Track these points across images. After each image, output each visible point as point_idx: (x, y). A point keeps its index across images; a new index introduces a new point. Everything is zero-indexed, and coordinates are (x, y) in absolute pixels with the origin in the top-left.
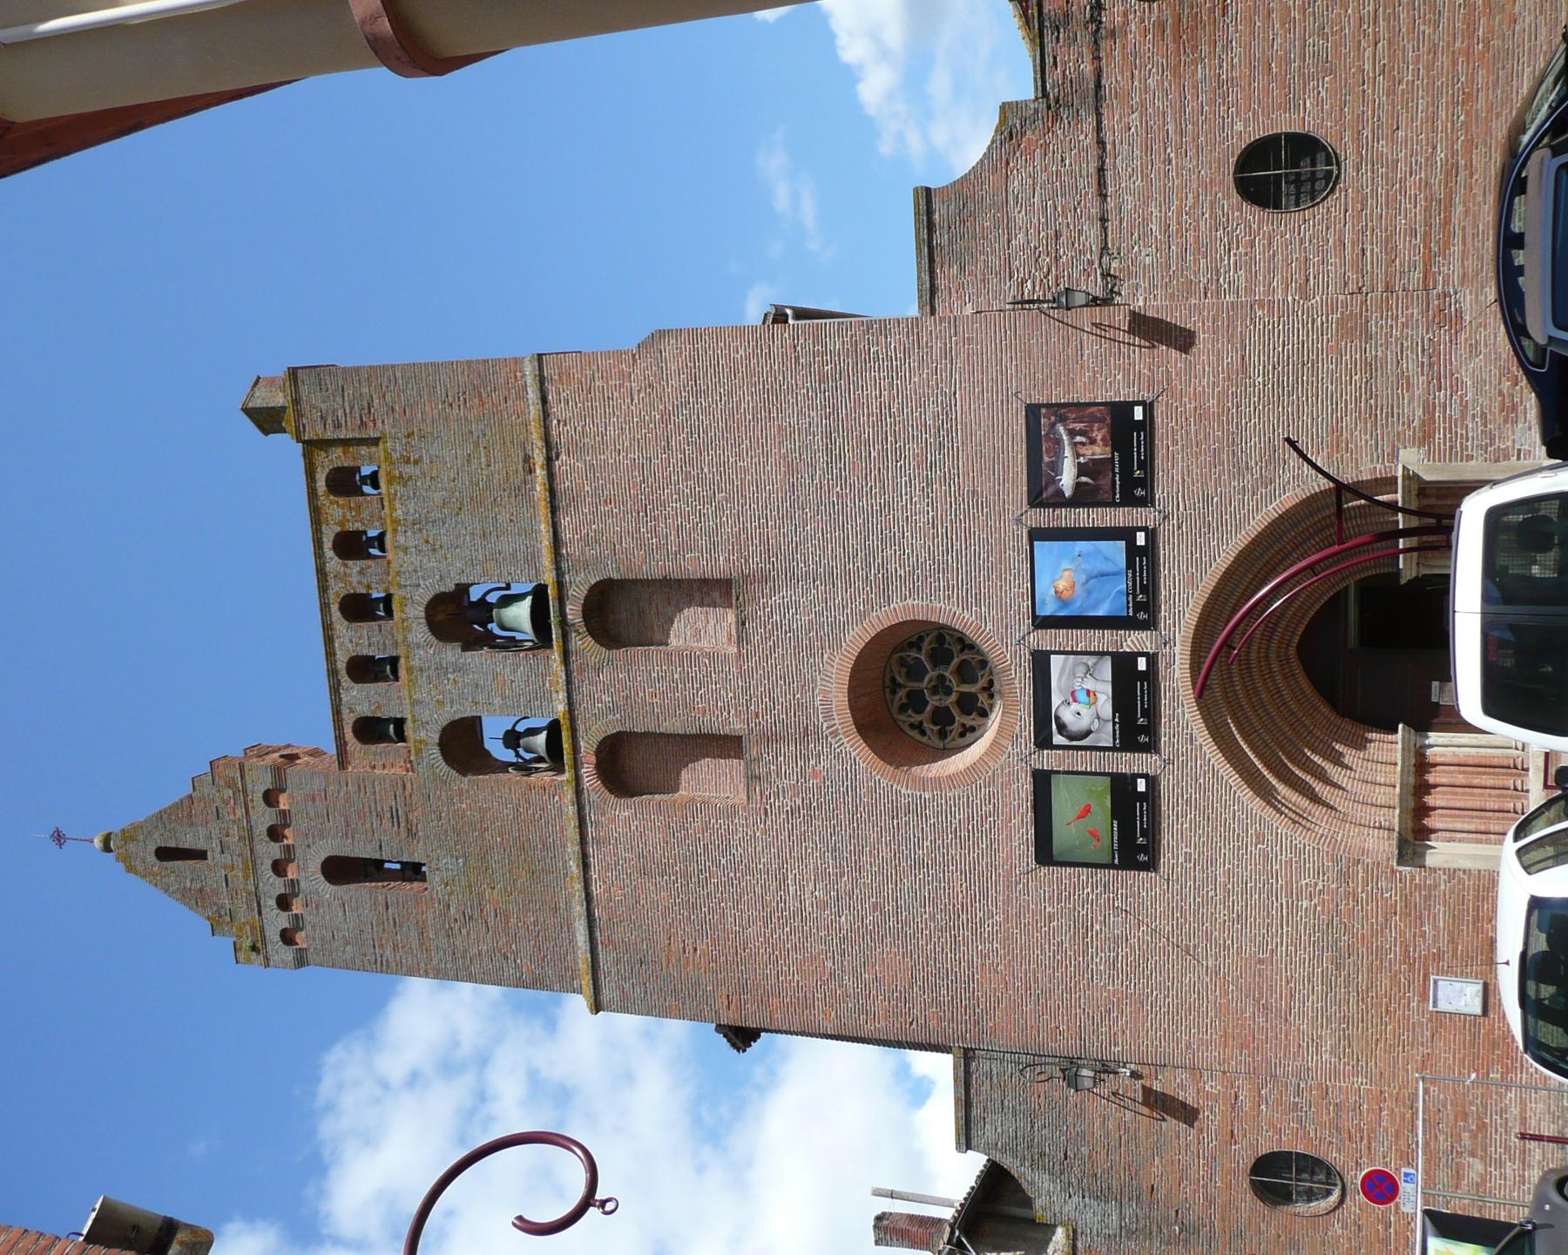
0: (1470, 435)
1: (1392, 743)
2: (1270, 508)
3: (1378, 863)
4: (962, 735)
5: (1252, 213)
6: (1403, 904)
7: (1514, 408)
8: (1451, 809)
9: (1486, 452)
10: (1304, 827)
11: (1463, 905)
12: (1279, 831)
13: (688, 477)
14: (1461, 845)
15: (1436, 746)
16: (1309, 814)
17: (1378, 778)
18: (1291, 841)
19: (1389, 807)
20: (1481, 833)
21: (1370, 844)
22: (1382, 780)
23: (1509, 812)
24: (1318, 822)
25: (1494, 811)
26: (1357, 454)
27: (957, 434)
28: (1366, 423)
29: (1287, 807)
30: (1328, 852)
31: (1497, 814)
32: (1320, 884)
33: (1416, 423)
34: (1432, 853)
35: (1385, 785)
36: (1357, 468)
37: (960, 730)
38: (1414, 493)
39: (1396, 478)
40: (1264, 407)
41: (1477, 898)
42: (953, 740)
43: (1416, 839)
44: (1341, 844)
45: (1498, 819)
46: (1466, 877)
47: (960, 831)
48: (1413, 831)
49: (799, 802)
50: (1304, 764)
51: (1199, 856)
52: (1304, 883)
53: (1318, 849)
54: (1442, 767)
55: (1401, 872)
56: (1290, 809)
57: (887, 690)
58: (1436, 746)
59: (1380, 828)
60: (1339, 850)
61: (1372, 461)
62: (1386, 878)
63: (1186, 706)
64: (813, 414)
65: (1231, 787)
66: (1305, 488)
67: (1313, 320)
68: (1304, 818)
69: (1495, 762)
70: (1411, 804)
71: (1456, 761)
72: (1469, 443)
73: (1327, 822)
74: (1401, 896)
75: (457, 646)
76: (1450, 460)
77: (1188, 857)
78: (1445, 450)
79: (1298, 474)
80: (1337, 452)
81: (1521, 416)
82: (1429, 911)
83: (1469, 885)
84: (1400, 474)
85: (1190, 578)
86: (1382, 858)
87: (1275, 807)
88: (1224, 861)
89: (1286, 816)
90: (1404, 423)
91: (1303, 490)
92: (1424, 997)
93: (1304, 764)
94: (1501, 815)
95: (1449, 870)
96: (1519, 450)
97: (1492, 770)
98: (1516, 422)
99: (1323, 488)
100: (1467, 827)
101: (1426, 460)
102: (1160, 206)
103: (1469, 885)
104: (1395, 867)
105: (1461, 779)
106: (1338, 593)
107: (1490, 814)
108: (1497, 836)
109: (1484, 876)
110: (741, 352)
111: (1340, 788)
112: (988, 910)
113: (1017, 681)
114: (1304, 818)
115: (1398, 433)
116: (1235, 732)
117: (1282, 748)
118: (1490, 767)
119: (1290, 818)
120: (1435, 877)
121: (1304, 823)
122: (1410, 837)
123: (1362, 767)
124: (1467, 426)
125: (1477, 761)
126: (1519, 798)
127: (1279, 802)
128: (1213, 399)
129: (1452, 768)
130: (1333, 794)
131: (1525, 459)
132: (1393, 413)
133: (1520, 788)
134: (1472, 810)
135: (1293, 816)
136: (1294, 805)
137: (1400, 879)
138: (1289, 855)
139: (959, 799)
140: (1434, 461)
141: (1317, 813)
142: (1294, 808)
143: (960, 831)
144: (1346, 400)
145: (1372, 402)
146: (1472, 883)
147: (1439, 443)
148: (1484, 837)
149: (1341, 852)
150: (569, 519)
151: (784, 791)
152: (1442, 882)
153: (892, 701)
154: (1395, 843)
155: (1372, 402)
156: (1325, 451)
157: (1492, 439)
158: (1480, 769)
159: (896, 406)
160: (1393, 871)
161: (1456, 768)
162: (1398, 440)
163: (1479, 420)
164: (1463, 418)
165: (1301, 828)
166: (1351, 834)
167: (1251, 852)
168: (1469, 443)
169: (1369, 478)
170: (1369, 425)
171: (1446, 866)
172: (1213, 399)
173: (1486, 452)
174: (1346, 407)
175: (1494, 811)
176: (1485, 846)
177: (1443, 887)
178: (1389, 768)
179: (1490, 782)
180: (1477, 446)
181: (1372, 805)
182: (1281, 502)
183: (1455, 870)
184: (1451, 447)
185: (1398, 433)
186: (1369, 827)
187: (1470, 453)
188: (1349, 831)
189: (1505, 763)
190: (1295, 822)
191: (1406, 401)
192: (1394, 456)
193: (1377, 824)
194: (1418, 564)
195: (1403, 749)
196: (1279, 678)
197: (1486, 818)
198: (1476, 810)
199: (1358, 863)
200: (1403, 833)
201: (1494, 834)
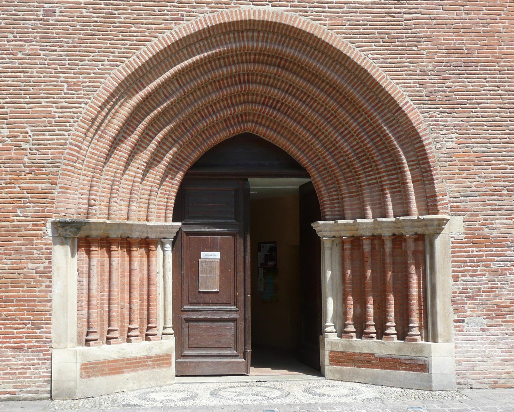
0: (476, 278)
1: (166, 217)
2: (408, 99)
3: (52, 203)
6: (10, 228)
7: (500, 316)
8: (110, 272)
9: (461, 292)
10: (88, 130)
11: (12, 287)
12: (83, 105)
14: (76, 283)
15: (130, 261)
16: (101, 136)
17: (135, 204)
19: (109, 214)
20: (89, 301)
21: (73, 195)
22: (134, 208)
23: (109, 325)
24: (92, 145)
25: (109, 311)
26: (458, 178)
28: (486, 186)
29: (107, 114)
30: (62, 153)
31: (106, 314)
32: (27, 146)
33: (486, 231)
34: (67, 252)
35: (129, 210)
36: (446, 178)
38: (420, 231)
39: (436, 213)
40: (500, 95)
41: (21, 299)
43: (80, 239)
44: (73, 166)
45: (102, 316)
46: (43, 288)
48: (88, 236)
50: (147, 134)
51: (52, 25)
52: (28, 129)
54: (146, 263)
55: (45, 225)
56: (105, 117)
58: (130, 261)
59: (89, 205)
60: (65, 164)
61: (452, 192)
62: (38, 211)
63: (211, 15)
65: (127, 58)
66: (427, 131)
68: (97, 130)
69: (153, 310)
70: (113, 235)
71: (153, 275)
72: (468, 278)
73: (93, 153)
74: (18, 226)
76: (453, 262)
78: (463, 257)
79: (440, 125)
80: (460, 161)
81: (493, 322)
82: (5, 254)
83: (35, 292)
84: (439, 216)
85: (340, 23)
86: (60, 207)
87: (107, 101)
88: (47, 50)
89: (99, 112)
90: (486, 220)
91: (425, 129)
93: (147, 134)
94: (106, 318)
95: (50, 272)
96: (463, 321)
97: (145, 307)
98: (487, 318)
99: (426, 147)
100: (94, 288)
101: (453, 240)
103: (35, 292)
104: (50, 220)
105: (136, 280)
106: (304, 170)
107: (106, 307)
108: (86, 315)
109: (45, 306)
111: (126, 168)
114: (97, 130)
115: (477, 215)
116: (194, 59)
117: (180, 100)
118: (149, 305)
119: (97, 116)
120: (40, 258)
121: (92, 130)
122: (82, 233)
123: (144, 189)
124: (483, 275)
125: (153, 293)
126: (122, 334)
127: (113, 107)
128: (508, 49)
129: (145, 272)
130: (119, 160)
131: (455, 327)
132: (495, 210)
133: (131, 334)
134: (110, 292)
135: (99, 120)
136: (110, 121)
137: (36, 225)
138: (57, 115)
140: (453, 247)
141: (101, 144)
142: (106, 121)
144: (506, 169)
145: (505, 192)
146: (37, 294)
147: (469, 251)
148: (85, 303)
149: (63, 166)
152: (35, 266)
154: (75, 218)
155: (505, 192)
156: (461, 150)
157: (473, 298)
158: (145, 297)
160: (44, 218)
161: (146, 276)
162: (472, 215)
163: (490, 285)
164: (491, 272)
165: (248, 27)
166: (82, 177)
167: (60, 77)
168: (468, 278)
169: (436, 190)
170: (484, 189)
171: (54, 269)
172: (508, 49)
173: (461, 292)
174: (500, 169)
175: (109, 311)
176: (76, 304)
177: (30, 266)
178: (143, 215)
179: (136, 307)
180: (466, 285)
181: (110, 198)
182: (414, 109)
183: (50, 277)
184: (465, 262)
185: (477, 215)
186: (90, 195)
187: (460, 278)
188: (85, 175)
189: (152, 319)
190: (93, 120)
191: (505, 221)
192: (457, 212)
193: (93, 202)
194: (334, 237)
195: (163, 227)
196: (228, 112)
197: (103, 304)
198: (110, 295)
199: (52, 184)
200: (87, 226)
201: (89, 314)
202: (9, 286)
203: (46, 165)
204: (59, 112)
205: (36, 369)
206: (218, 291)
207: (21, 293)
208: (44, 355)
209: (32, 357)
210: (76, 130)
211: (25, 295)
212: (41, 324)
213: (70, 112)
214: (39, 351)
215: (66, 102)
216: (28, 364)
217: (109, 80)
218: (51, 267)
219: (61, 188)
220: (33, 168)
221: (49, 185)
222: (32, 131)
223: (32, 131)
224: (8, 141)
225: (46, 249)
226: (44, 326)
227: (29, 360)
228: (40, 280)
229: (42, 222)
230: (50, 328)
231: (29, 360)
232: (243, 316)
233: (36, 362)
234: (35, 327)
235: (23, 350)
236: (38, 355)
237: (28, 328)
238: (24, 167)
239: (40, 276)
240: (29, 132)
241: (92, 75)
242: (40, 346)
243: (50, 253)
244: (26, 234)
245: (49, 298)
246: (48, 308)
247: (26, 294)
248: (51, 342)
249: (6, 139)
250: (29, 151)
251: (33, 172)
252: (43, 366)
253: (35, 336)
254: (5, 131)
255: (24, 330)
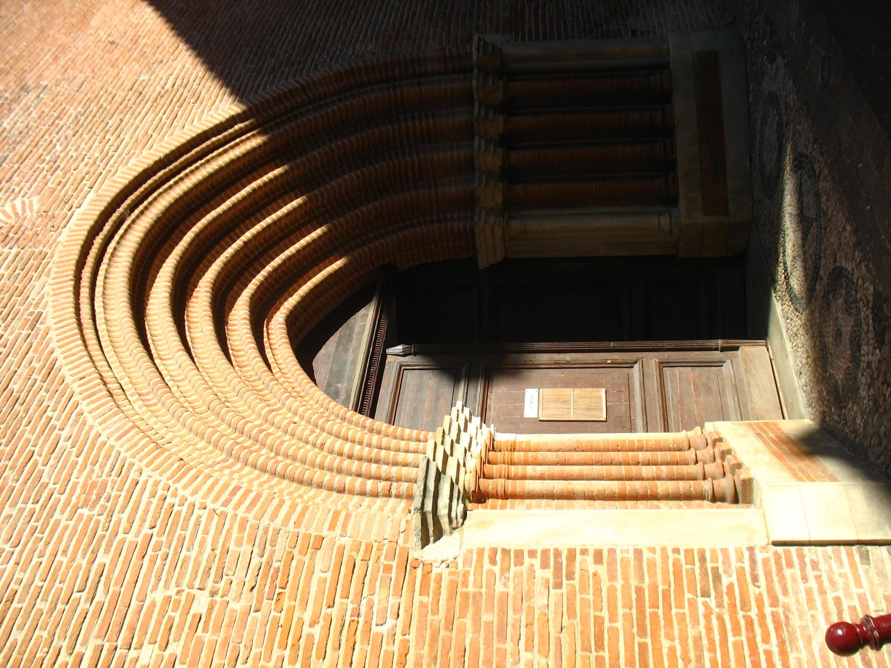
46: (602, 570)
52: (158, 596)
83: (612, 590)
103: (612, 590)
104: (416, 553)
109: (652, 564)
146: (619, 583)
149: (278, 522)
171: (551, 544)
183: (572, 553)
202: (597, 658)
203: (264, 560)
204: (141, 526)
205: (832, 582)
206: (603, 390)
207: (619, 625)
208: (790, 565)
209: (803, 597)
210: (195, 492)
211: (624, 615)
212: (704, 573)
213: (149, 503)
214: (782, 579)
215: (122, 511)
216: (824, 603)
217: (104, 430)
218: (545, 552)
219: (332, 527)
220: (267, 589)
221: (320, 553)
222: (166, 587)
223: (166, 587)
224: (175, 648)
225: (493, 561)
226: (709, 565)
227: (810, 601)
228: (582, 577)
229: (419, 572)
230: (713, 552)
231: (810, 601)
232: (651, 354)
233: (813, 584)
234: (715, 588)
235: (787, 617)
236: (794, 580)
237: (720, 605)
238: (257, 611)
239: (570, 576)
240: (168, 593)
241: (81, 460)
242: (768, 574)
243: (506, 552)
244: (448, 611)
245: (631, 555)
246: (658, 557)
247: (621, 611)
248: (751, 549)
249: (167, 653)
250: (217, 598)
251: (278, 590)
252: (823, 566)
253: (740, 586)
254: (148, 653)
255: (727, 618)
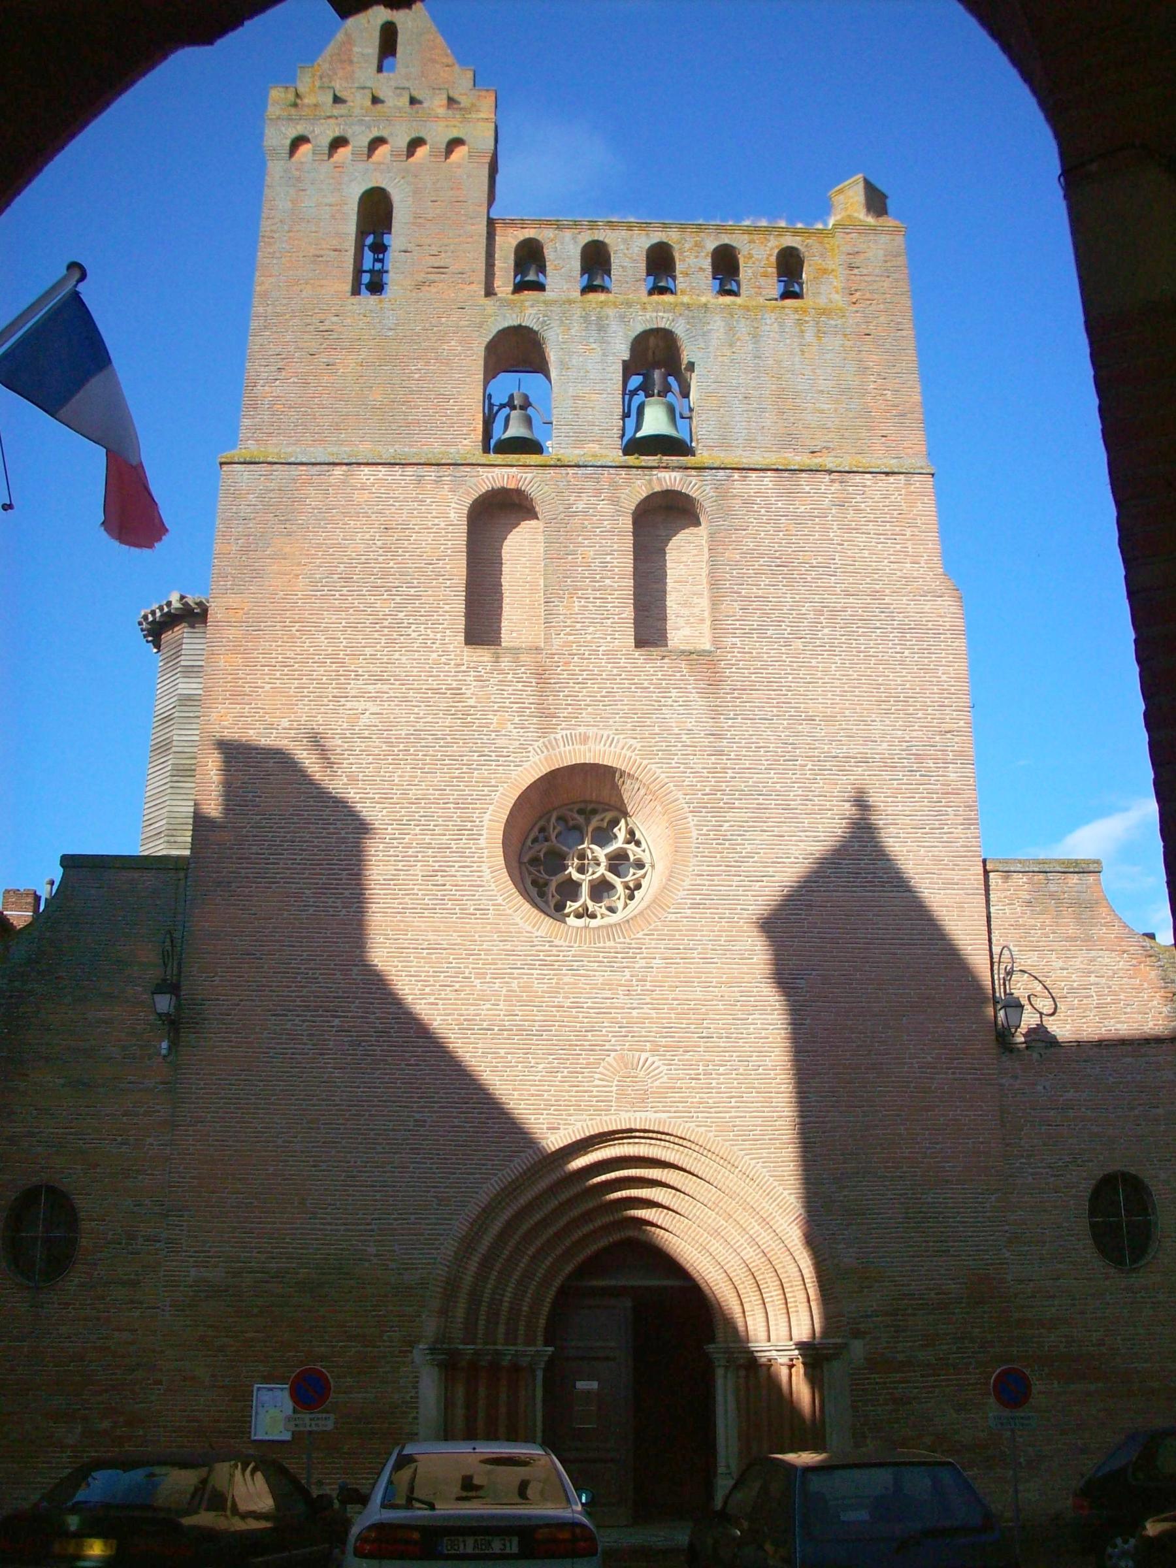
4: (535, 883)
5: (1086, 1188)
13: (820, 612)
18: (442, 1235)
27: (870, 891)
37: (541, 881)
42: (530, 873)
47: (442, 876)
49: (472, 702)
53: (434, 1264)
57: (582, 806)
64: (885, 745)
67: (987, 1251)
75: (626, 357)
77: (421, 1123)
92: (268, 1379)
102: (1090, 1100)
110: (944, 678)
112: (353, 903)
113: (612, 944)
139: (479, 877)
143: (442, 876)
150: (770, 486)
151: (483, 687)
153: (571, 810)
159: (896, 831)
